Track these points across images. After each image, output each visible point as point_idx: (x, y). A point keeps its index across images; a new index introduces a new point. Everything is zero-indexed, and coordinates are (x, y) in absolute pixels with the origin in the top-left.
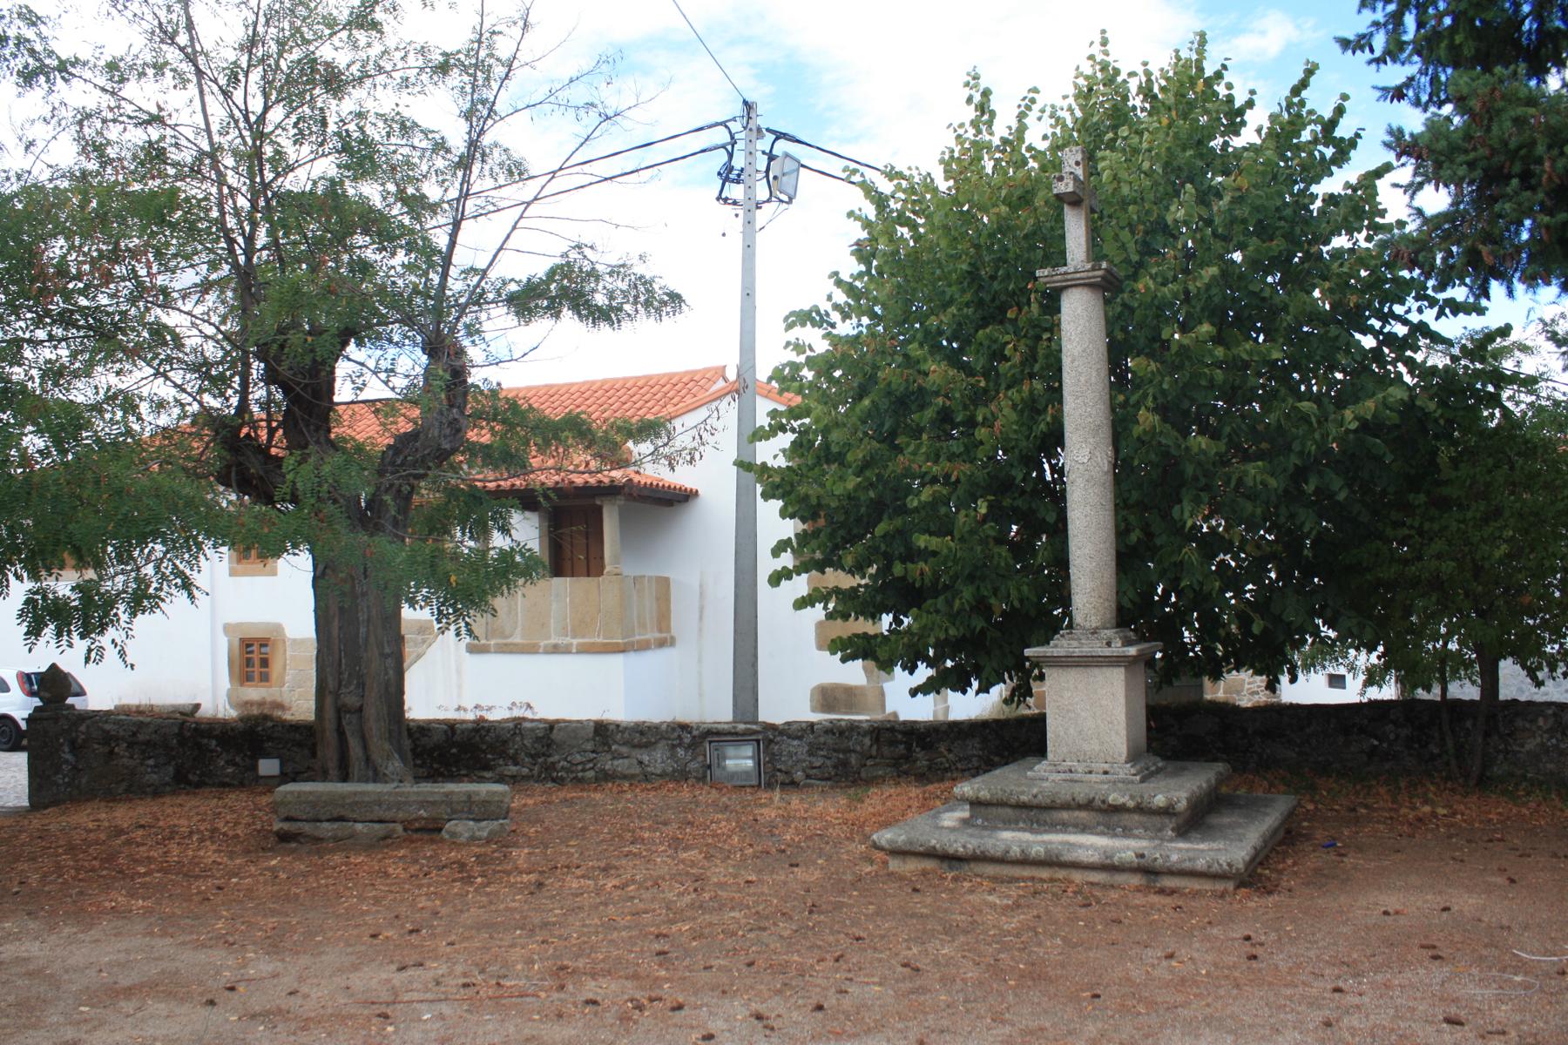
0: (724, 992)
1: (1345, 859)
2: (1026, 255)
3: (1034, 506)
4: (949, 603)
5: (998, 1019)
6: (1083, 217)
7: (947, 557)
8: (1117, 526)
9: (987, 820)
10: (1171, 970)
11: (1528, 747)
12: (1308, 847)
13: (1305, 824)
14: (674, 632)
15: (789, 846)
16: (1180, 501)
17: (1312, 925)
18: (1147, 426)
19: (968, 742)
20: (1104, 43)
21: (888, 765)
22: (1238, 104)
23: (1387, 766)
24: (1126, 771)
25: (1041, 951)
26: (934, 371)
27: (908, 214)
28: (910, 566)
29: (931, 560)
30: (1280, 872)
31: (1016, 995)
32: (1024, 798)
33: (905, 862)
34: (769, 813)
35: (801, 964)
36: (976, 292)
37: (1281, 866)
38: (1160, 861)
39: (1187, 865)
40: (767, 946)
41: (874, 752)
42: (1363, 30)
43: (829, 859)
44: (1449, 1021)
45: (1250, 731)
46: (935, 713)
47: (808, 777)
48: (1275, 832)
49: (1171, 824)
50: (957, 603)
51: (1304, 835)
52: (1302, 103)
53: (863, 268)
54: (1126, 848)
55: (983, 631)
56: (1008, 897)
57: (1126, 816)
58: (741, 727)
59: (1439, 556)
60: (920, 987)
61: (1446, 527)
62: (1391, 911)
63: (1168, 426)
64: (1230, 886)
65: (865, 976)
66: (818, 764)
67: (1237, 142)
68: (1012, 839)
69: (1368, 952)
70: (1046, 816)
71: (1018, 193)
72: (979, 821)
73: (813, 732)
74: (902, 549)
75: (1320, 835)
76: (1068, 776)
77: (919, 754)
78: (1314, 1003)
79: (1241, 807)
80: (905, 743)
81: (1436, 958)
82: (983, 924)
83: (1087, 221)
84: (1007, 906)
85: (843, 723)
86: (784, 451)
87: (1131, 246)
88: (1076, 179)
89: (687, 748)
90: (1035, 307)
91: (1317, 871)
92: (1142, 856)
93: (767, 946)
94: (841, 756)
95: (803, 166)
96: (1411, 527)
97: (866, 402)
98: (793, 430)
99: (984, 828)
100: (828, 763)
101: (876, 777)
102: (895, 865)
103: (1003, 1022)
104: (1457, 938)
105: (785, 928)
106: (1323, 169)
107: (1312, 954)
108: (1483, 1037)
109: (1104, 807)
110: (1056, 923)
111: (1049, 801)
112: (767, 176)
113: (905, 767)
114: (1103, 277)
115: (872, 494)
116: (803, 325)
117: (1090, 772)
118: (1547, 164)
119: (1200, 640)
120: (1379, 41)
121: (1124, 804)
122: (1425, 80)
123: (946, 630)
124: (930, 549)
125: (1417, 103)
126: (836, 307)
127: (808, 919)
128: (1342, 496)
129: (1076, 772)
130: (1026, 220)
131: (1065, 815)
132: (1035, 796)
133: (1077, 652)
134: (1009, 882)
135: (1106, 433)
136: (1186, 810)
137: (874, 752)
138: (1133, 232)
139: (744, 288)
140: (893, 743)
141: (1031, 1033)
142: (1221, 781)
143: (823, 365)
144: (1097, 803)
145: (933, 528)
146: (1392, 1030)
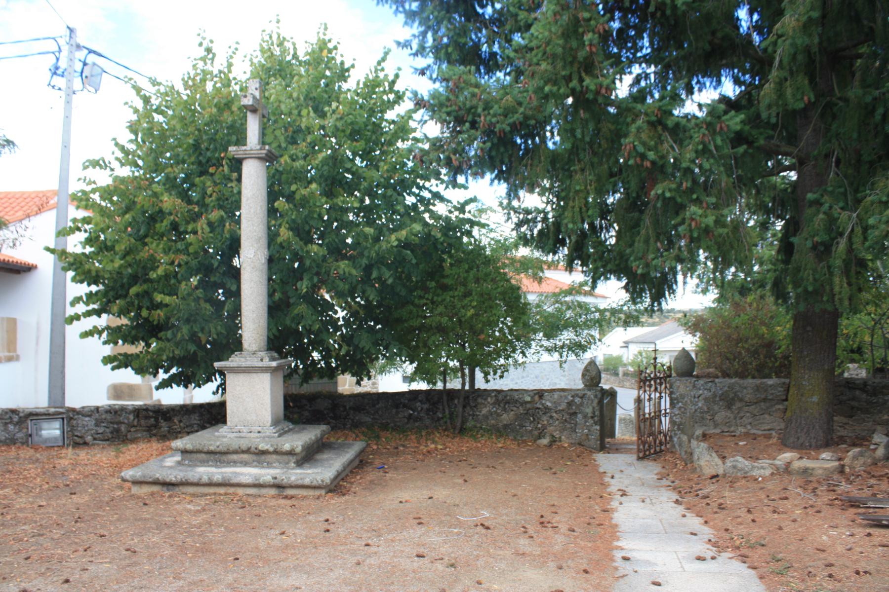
0: (706, 522)
2: (226, 138)
4: (175, 335)
5: (177, 577)
10: (282, 541)
11: (483, 412)
12: (369, 469)
14: (19, 352)
15: (72, 482)
16: (302, 279)
18: (285, 237)
20: (326, 29)
22: (346, 66)
23: (417, 424)
24: (270, 431)
25: (210, 535)
27: (163, 108)
29: (165, 309)
30: (352, 483)
31: (191, 562)
32: (212, 448)
34: (64, 462)
35: (62, 555)
36: (198, 157)
39: (300, 482)
40: (42, 545)
41: (135, 423)
42: (408, 38)
43: (96, 488)
44: (418, 556)
46: (184, 400)
47: (95, 439)
48: (351, 461)
50: (179, 335)
52: (383, 70)
53: (133, 137)
54: (266, 474)
55: (195, 352)
56: (199, 505)
57: (269, 456)
58: (52, 410)
59: (441, 314)
60: (134, 562)
61: (444, 300)
62: (404, 500)
63: (298, 239)
64: (323, 492)
65: (103, 558)
66: (100, 431)
67: (345, 86)
68: (205, 472)
69: (387, 523)
70: (224, 458)
71: (224, 101)
72: (187, 462)
74: (148, 304)
75: (378, 462)
77: (163, 423)
78: (353, 553)
79: (334, 449)
81: (420, 523)
84: (198, 511)
86: (81, 243)
87: (282, 139)
88: (254, 97)
89: (16, 424)
90: (226, 168)
91: (371, 482)
92: (276, 478)
93: (42, 545)
94: (115, 426)
96: (427, 299)
97: (127, 216)
98: (86, 231)
99: (190, 466)
100: (108, 430)
102: (135, 490)
103: (180, 579)
104: (433, 512)
105: (57, 533)
106: (391, 105)
107: (358, 527)
108: (432, 562)
113: (154, 432)
114: (266, 154)
115: (130, 270)
116: (94, 167)
118: (482, 118)
119: (323, 358)
120: (415, 46)
122: (436, 67)
123: (173, 352)
125: (431, 78)
126: (117, 159)
127: (73, 526)
128: (390, 281)
130: (227, 118)
131: (235, 457)
133: (244, 365)
135: (264, 241)
136: (302, 451)
137: (135, 423)
138: (286, 130)
139: (63, 142)
140: (147, 418)
141: (195, 583)
143: (106, 193)
144: (253, 449)
146: (390, 564)
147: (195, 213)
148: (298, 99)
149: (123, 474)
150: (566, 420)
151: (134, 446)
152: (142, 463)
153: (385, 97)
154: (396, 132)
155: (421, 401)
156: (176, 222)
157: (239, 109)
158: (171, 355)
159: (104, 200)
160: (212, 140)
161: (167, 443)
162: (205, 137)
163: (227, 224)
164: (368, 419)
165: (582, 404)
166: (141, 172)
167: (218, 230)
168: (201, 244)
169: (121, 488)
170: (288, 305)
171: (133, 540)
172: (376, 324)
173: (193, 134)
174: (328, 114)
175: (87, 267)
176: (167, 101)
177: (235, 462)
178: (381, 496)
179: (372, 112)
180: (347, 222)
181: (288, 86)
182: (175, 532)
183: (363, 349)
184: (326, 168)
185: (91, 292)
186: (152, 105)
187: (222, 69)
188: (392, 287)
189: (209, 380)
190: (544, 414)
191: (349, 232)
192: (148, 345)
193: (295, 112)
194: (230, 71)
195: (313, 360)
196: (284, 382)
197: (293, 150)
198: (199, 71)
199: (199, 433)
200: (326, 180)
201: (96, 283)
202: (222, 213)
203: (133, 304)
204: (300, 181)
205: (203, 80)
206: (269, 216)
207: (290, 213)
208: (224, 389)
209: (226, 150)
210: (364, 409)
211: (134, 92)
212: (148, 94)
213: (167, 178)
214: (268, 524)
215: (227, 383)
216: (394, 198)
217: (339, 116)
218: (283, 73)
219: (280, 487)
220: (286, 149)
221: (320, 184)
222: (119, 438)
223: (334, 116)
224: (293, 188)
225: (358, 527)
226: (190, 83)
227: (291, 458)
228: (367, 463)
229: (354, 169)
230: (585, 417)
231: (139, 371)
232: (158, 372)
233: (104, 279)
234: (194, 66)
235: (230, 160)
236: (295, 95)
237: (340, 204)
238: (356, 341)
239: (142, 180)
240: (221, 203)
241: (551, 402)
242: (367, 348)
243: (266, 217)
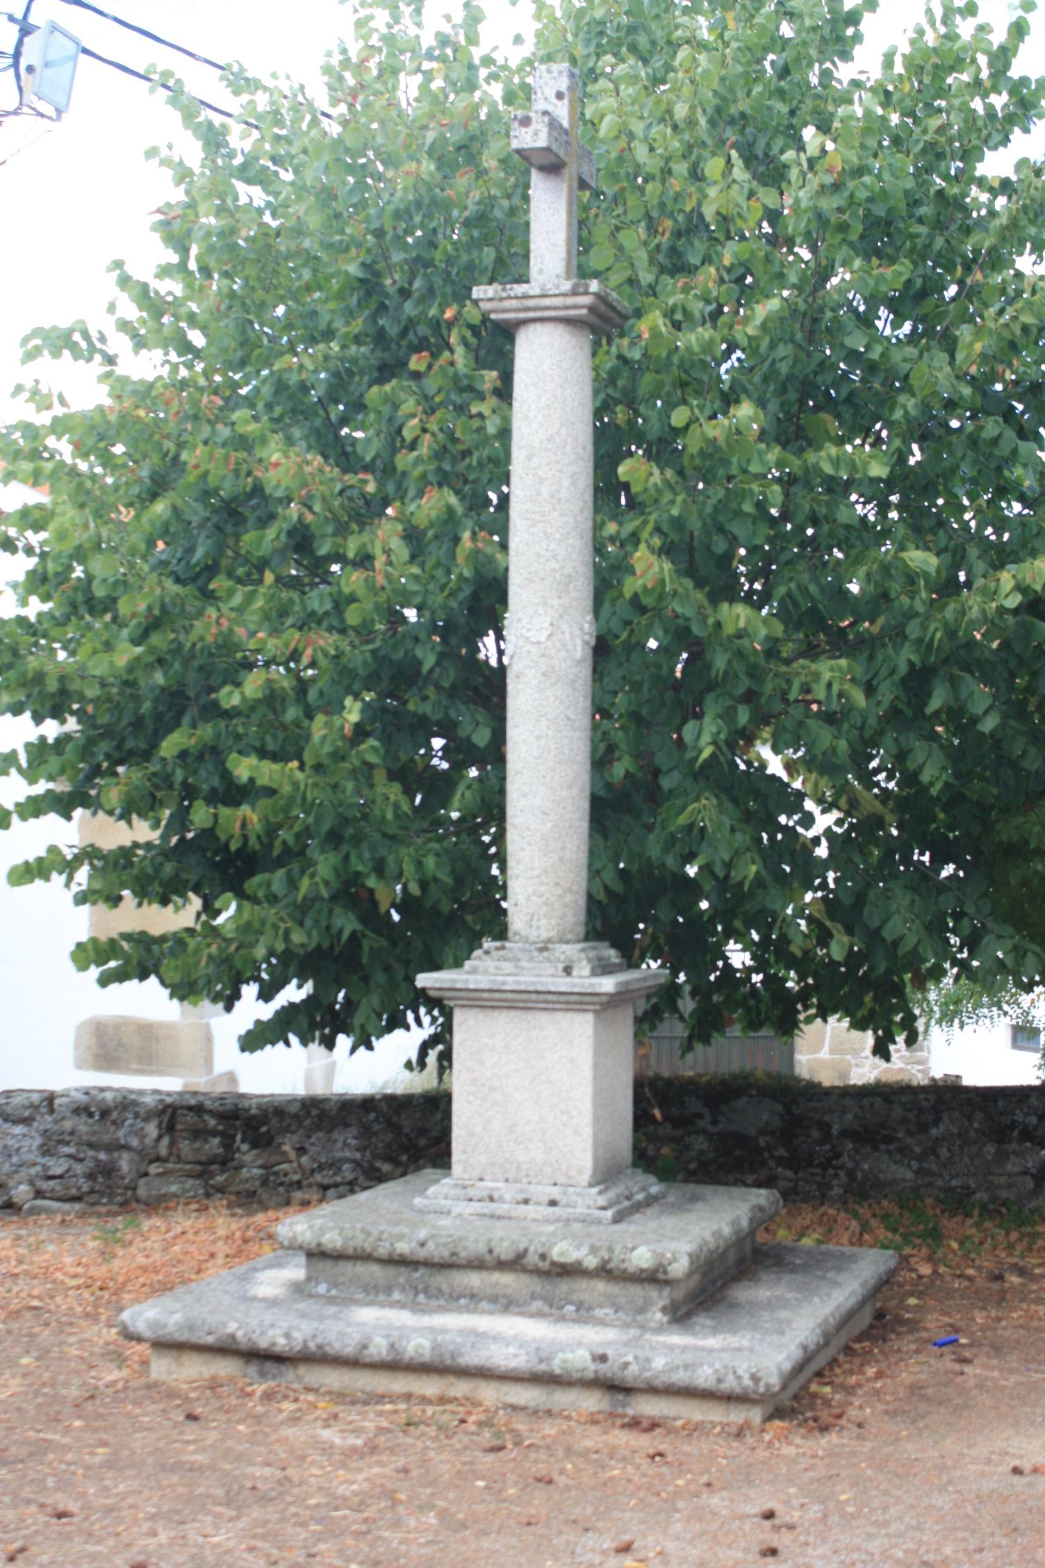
1: (967, 1369)
2: (465, 258)
3: (452, 714)
4: (293, 884)
6: (564, 194)
7: (291, 799)
8: (594, 751)
9: (335, 1285)
12: (907, 1344)
13: (912, 1301)
16: (699, 716)
17: (886, 1493)
19: (335, 1135)
21: (190, 1175)
25: (394, 1536)
26: (277, 465)
28: (224, 811)
29: (264, 802)
30: (850, 1390)
32: (403, 1247)
33: (180, 1365)
36: (374, 318)
37: (853, 1380)
38: (634, 1369)
39: (681, 1378)
41: (163, 1148)
45: (836, 1129)
46: (308, 1081)
47: (39, 1194)
48: (849, 1317)
49: (660, 1298)
50: (305, 884)
51: (908, 1321)
53: (175, 258)
56: (357, 1431)
62: (1027, 1467)
63: (688, 583)
64: (755, 1415)
66: (58, 1171)
67: (845, 73)
69: (973, 1544)
70: (442, 1280)
72: (322, 1289)
73: (52, 1111)
74: (216, 781)
75: (934, 1322)
76: (487, 1207)
77: (247, 1155)
79: (794, 1269)
80: (222, 1134)
82: (301, 1484)
83: (570, 204)
84: (354, 1449)
85: (109, 1096)
86: (15, 586)
87: (642, 256)
88: (553, 124)
91: (915, 1389)
92: (603, 1358)
94: (102, 1156)
95: (86, 51)
97: (160, 507)
98: (29, 551)
99: (331, 1300)
100: (79, 1168)
101: (164, 1197)
102: (162, 1368)
107: (875, 1546)
109: (544, 1266)
110: (433, 1483)
111: (446, 1253)
112: (16, 65)
113: (220, 1179)
114: (591, 309)
115: (159, 678)
117: (526, 1202)
121: (579, 1263)
123: (287, 934)
124: (259, 782)
126: (124, 326)
128: (989, 724)
129: (501, 1200)
131: (474, 1279)
132: (423, 1244)
133: (511, 983)
134: (366, 1403)
135: (583, 589)
136: (689, 1275)
138: (652, 229)
140: (199, 1134)
142: (762, 1221)
144: (532, 1259)
145: (271, 746)
147: (363, 495)
148: (691, 122)
149: (125, 1316)
151: (156, 1221)
152: (185, 1281)
153: (977, 105)
154: (1014, 224)
156: (307, 527)
157: (503, 161)
158: (280, 947)
159: (85, 456)
160: (419, 264)
161: (260, 1218)
162: (397, 257)
163: (466, 535)
164: (904, 1173)
166: (200, 367)
167: (436, 552)
168: (382, 597)
169: (120, 1359)
170: (655, 797)
171: (154, 1534)
172: (939, 860)
173: (359, 246)
174: (794, 174)
175: (32, 663)
176: (278, 138)
178: (950, 1443)
179: (934, 155)
180: (848, 527)
181: (657, 80)
182: (282, 1520)
183: (896, 944)
184: (783, 350)
185: (43, 739)
186: (231, 155)
187: (447, 29)
188: (996, 739)
189: (397, 1022)
191: (855, 560)
192: (210, 909)
193: (681, 168)
194: (473, 40)
195: (728, 968)
196: (639, 1039)
197: (674, 292)
198: (374, 41)
199: (363, 1196)
200: (783, 389)
201: (57, 713)
202: (453, 500)
203: (167, 779)
204: (698, 393)
205: (390, 71)
206: (597, 509)
207: (667, 496)
208: (446, 1058)
209: (462, 295)
210: (889, 1140)
211: (177, 116)
212: (217, 119)
213: (280, 386)
214: (576, 1512)
215: (458, 1038)
216: (1004, 449)
217: (829, 179)
218: (642, 40)
219: (616, 1387)
220: (652, 290)
221: (761, 403)
222: (111, 1196)
223: (814, 181)
224: (679, 417)
225: (875, 1546)
226: (350, 80)
227: (653, 1292)
228: (900, 1321)
229: (875, 355)
231: (184, 990)
232: (236, 995)
233: (81, 698)
234: (360, 24)
235: (472, 327)
236: (681, 111)
237: (828, 469)
238: (871, 917)
239: (201, 390)
240: (447, 467)
242: (910, 942)
243: (588, 513)
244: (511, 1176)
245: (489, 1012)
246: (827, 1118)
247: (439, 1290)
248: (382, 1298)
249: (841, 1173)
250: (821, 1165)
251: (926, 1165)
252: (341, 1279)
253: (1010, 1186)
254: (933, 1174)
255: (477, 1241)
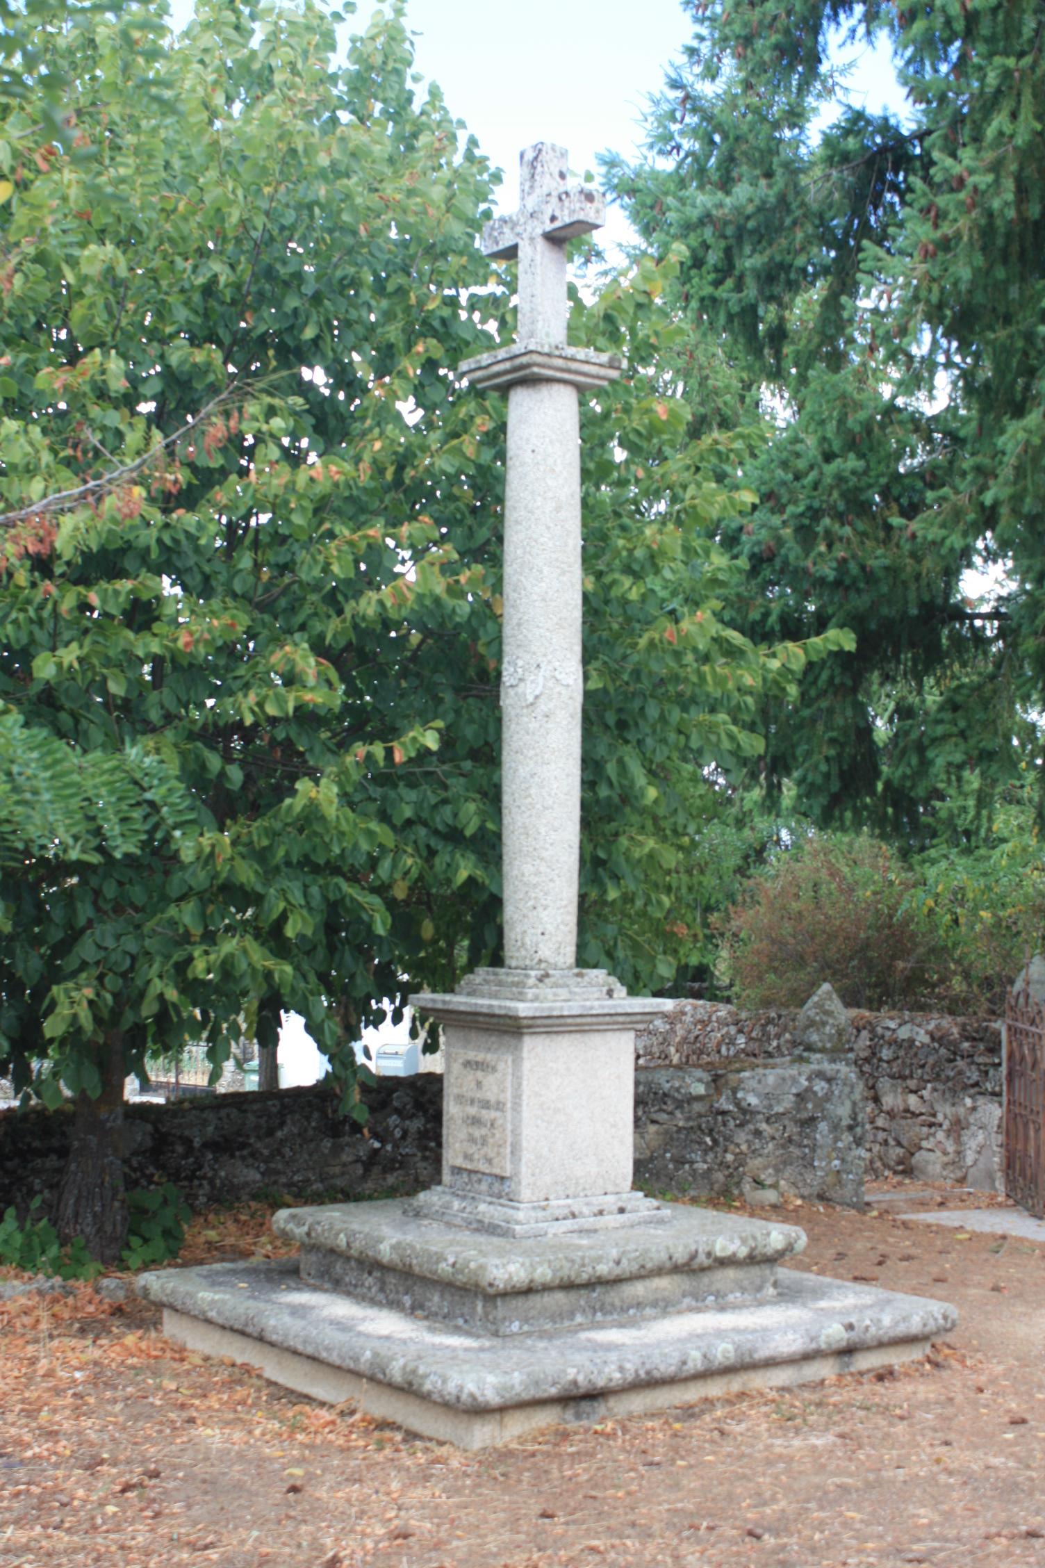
9: (526, 1320)
39: (902, 1330)
45: (197, 1142)
70: (614, 1296)
76: (569, 1224)
117: (601, 1213)
129: (582, 1215)
131: (639, 1289)
132: (618, 1263)
150: (790, 1140)
155: (398, 1111)
165: (828, 1098)
177: (639, 1305)
190: (741, 1125)
210: (243, 1146)
230: (835, 1127)
241: (758, 1095)
244: (570, 1192)
245: (554, 1036)
246: (187, 1133)
247: (613, 1305)
248: (567, 1323)
249: (205, 1182)
250: (186, 1178)
251: (272, 1165)
252: (532, 1313)
253: (343, 1174)
254: (278, 1173)
255: (658, 1251)
